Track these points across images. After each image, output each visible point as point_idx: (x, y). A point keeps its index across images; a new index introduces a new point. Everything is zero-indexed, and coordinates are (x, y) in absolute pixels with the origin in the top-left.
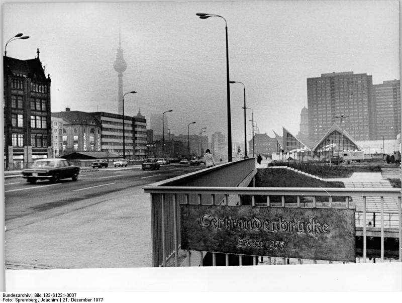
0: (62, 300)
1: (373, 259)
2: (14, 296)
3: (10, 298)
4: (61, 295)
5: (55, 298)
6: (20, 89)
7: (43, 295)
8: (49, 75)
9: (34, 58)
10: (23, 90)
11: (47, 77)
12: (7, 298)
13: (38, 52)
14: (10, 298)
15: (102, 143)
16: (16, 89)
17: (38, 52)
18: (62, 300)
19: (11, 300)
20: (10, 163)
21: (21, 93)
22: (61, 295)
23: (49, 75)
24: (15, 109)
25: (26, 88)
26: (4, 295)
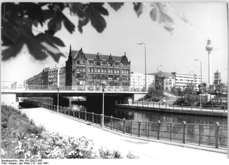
0: (32, 163)
1: (215, 136)
2: (8, 161)
3: (6, 162)
4: (36, 160)
5: (29, 162)
6: (118, 67)
7: (43, 163)
8: (130, 61)
9: (123, 55)
10: (119, 67)
11: (129, 61)
12: (4, 162)
13: (125, 53)
14: (6, 162)
15: (108, 81)
16: (117, 67)
17: (125, 53)
18: (32, 163)
19: (6, 164)
20: (2, 81)
21: (118, 68)
22: (36, 160)
23: (130, 61)
24: (110, 73)
25: (120, 66)
26: (2, 160)
